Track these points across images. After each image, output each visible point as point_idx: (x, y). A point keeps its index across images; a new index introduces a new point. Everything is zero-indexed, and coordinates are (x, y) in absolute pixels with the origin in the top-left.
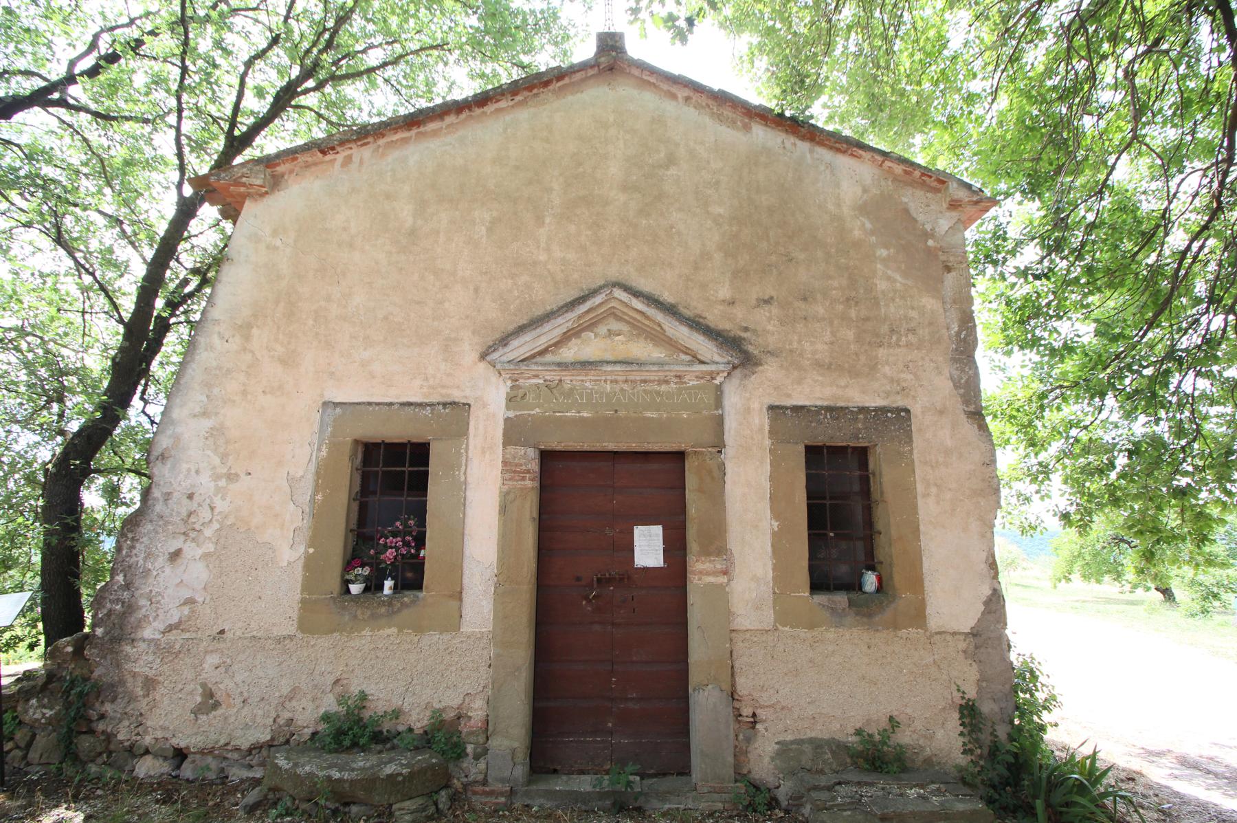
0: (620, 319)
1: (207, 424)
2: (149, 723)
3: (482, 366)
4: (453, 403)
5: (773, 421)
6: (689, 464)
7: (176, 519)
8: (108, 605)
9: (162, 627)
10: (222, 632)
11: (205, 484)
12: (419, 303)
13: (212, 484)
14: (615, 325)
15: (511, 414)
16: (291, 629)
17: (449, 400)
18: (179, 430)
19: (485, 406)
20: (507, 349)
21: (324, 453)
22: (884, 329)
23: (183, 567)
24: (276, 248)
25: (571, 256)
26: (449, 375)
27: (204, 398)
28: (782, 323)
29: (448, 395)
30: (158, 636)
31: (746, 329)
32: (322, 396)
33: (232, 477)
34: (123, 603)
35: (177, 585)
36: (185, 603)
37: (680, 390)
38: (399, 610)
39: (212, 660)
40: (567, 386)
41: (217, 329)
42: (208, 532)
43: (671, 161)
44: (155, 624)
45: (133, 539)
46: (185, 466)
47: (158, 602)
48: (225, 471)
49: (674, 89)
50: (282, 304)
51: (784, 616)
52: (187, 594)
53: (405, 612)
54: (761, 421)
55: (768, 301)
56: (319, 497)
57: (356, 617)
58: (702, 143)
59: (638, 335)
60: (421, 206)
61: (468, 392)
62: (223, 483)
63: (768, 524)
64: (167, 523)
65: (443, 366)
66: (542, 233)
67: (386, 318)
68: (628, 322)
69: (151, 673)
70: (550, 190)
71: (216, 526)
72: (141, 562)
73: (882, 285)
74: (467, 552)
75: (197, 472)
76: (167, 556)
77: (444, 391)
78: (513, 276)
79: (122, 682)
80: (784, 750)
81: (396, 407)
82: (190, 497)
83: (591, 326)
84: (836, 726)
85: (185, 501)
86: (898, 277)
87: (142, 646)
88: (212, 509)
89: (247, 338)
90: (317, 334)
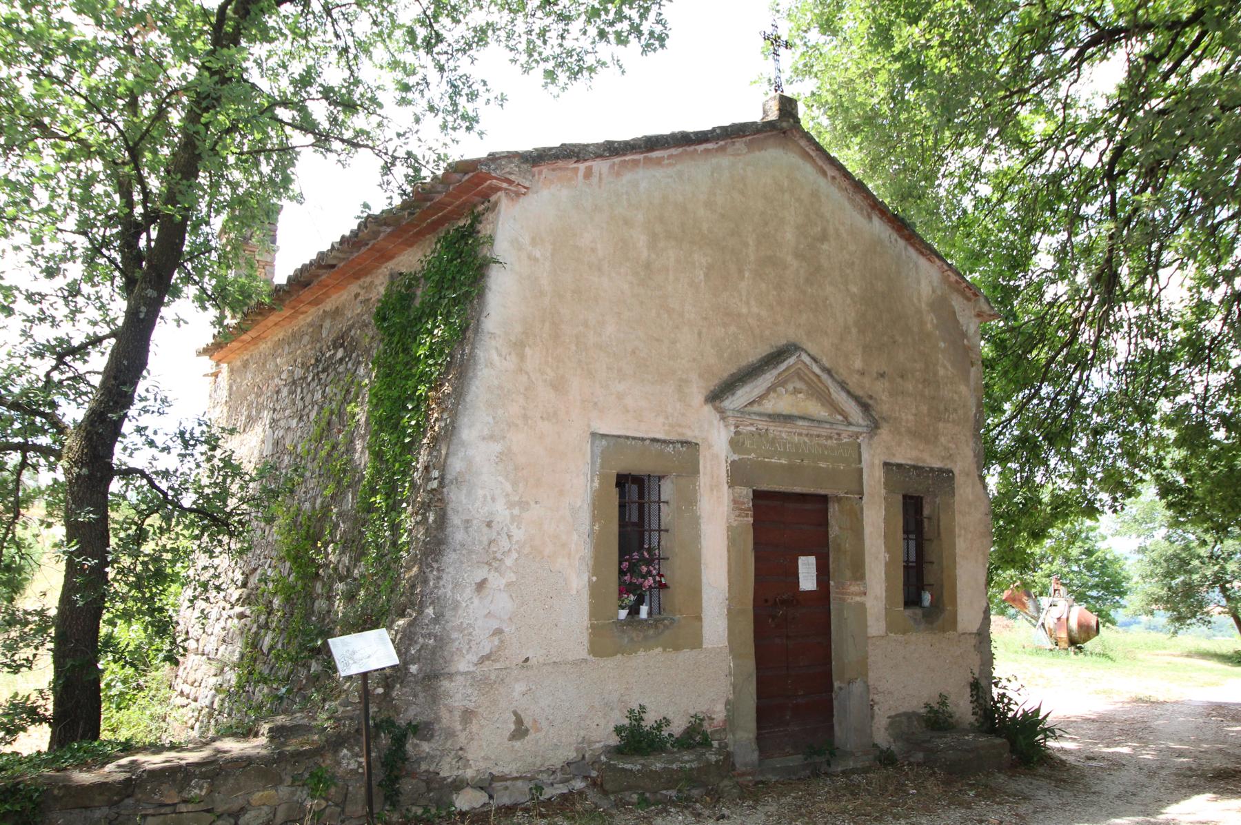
0: (801, 379)
1: (497, 447)
2: (470, 756)
3: (708, 409)
4: (686, 442)
5: (886, 474)
6: (833, 509)
7: (478, 548)
8: (421, 640)
9: (475, 659)
10: (527, 659)
11: (501, 510)
12: (657, 340)
13: (507, 512)
14: (799, 385)
15: (736, 457)
16: (583, 653)
17: (683, 439)
18: (471, 452)
19: (710, 446)
20: (735, 398)
21: (596, 484)
22: (942, 407)
23: (490, 598)
24: (536, 260)
25: (764, 313)
26: (683, 415)
27: (490, 419)
28: (891, 395)
29: (683, 434)
30: (472, 669)
31: (871, 397)
32: (589, 426)
33: (524, 505)
34: (436, 637)
35: (486, 616)
36: (493, 634)
37: (839, 445)
38: (663, 631)
39: (520, 687)
40: (771, 436)
41: (493, 343)
42: (509, 562)
43: (824, 237)
44: (469, 657)
45: (438, 569)
46: (480, 492)
47: (470, 634)
48: (517, 499)
49: (827, 167)
50: (547, 324)
51: (892, 626)
52: (495, 625)
53: (667, 632)
54: (879, 473)
55: (882, 375)
56: (596, 528)
57: (632, 639)
58: (843, 224)
59: (812, 395)
60: (653, 239)
61: (697, 433)
62: (516, 511)
63: (883, 556)
64: (471, 552)
65: (678, 405)
66: (743, 285)
67: (633, 352)
68: (806, 383)
69: (471, 706)
70: (746, 245)
71: (515, 555)
72: (449, 594)
73: (941, 372)
74: (704, 579)
75: (493, 499)
76: (474, 587)
77: (680, 430)
78: (725, 325)
79: (438, 719)
80: (894, 720)
81: (648, 442)
82: (489, 525)
83: (783, 383)
84: (915, 703)
85: (485, 529)
86: (949, 367)
87: (460, 680)
88: (509, 537)
89: (522, 357)
90: (580, 361)
